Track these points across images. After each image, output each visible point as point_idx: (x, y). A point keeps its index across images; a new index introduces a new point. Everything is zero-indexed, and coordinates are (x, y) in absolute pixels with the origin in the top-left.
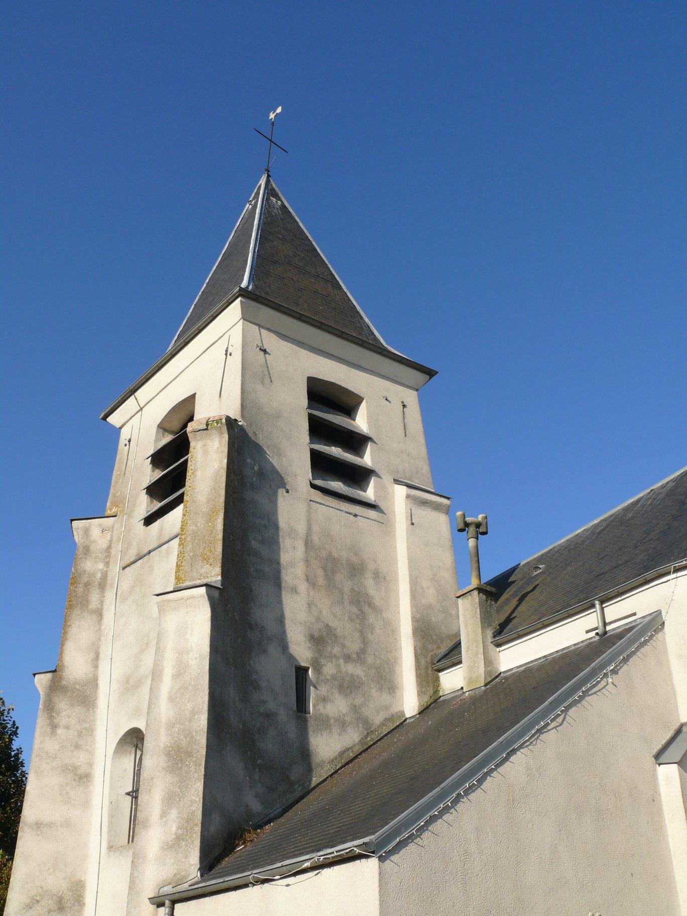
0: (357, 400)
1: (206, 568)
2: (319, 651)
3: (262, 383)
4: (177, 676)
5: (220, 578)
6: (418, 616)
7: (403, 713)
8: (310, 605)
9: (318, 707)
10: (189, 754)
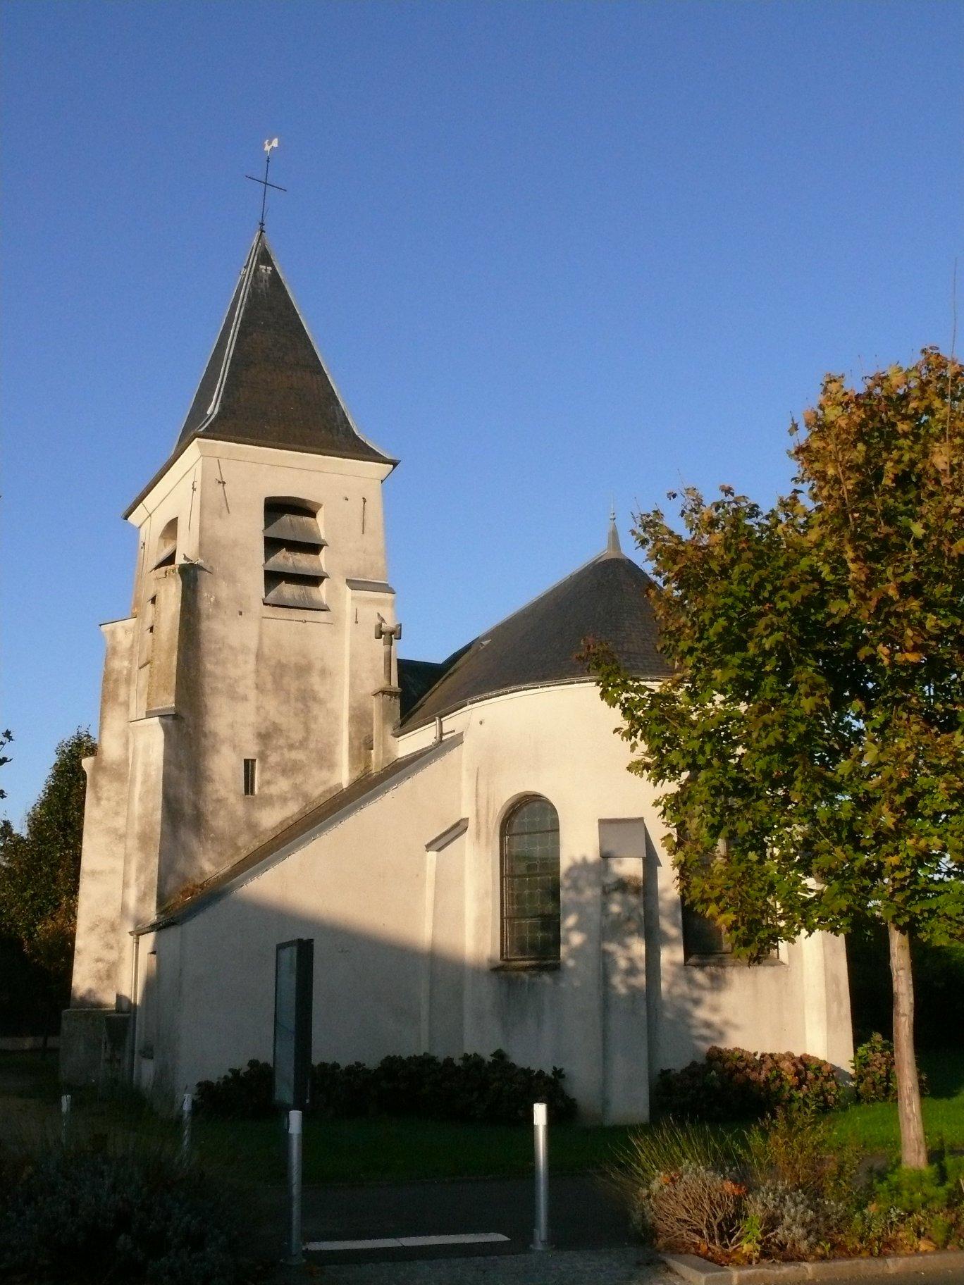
2: (265, 745)
3: (220, 516)
4: (144, 782)
5: (174, 705)
6: (355, 705)
7: (340, 785)
8: (258, 709)
9: (263, 789)
10: (151, 839)
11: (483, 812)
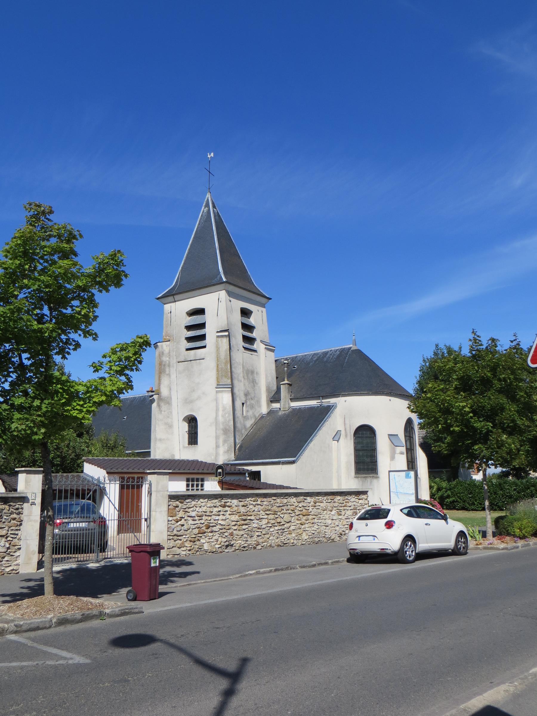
0: (251, 312)
1: (225, 380)
4: (223, 410)
11: (348, 429)
